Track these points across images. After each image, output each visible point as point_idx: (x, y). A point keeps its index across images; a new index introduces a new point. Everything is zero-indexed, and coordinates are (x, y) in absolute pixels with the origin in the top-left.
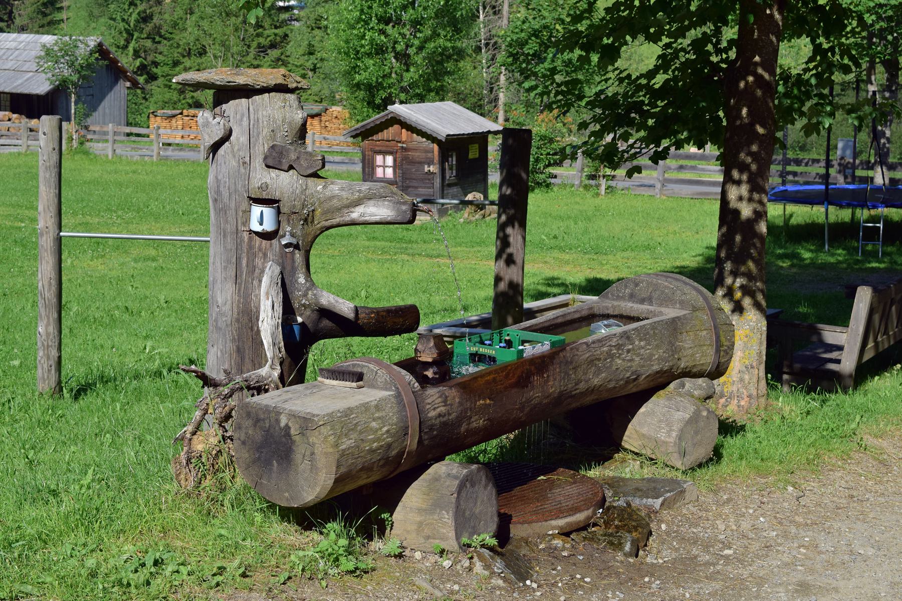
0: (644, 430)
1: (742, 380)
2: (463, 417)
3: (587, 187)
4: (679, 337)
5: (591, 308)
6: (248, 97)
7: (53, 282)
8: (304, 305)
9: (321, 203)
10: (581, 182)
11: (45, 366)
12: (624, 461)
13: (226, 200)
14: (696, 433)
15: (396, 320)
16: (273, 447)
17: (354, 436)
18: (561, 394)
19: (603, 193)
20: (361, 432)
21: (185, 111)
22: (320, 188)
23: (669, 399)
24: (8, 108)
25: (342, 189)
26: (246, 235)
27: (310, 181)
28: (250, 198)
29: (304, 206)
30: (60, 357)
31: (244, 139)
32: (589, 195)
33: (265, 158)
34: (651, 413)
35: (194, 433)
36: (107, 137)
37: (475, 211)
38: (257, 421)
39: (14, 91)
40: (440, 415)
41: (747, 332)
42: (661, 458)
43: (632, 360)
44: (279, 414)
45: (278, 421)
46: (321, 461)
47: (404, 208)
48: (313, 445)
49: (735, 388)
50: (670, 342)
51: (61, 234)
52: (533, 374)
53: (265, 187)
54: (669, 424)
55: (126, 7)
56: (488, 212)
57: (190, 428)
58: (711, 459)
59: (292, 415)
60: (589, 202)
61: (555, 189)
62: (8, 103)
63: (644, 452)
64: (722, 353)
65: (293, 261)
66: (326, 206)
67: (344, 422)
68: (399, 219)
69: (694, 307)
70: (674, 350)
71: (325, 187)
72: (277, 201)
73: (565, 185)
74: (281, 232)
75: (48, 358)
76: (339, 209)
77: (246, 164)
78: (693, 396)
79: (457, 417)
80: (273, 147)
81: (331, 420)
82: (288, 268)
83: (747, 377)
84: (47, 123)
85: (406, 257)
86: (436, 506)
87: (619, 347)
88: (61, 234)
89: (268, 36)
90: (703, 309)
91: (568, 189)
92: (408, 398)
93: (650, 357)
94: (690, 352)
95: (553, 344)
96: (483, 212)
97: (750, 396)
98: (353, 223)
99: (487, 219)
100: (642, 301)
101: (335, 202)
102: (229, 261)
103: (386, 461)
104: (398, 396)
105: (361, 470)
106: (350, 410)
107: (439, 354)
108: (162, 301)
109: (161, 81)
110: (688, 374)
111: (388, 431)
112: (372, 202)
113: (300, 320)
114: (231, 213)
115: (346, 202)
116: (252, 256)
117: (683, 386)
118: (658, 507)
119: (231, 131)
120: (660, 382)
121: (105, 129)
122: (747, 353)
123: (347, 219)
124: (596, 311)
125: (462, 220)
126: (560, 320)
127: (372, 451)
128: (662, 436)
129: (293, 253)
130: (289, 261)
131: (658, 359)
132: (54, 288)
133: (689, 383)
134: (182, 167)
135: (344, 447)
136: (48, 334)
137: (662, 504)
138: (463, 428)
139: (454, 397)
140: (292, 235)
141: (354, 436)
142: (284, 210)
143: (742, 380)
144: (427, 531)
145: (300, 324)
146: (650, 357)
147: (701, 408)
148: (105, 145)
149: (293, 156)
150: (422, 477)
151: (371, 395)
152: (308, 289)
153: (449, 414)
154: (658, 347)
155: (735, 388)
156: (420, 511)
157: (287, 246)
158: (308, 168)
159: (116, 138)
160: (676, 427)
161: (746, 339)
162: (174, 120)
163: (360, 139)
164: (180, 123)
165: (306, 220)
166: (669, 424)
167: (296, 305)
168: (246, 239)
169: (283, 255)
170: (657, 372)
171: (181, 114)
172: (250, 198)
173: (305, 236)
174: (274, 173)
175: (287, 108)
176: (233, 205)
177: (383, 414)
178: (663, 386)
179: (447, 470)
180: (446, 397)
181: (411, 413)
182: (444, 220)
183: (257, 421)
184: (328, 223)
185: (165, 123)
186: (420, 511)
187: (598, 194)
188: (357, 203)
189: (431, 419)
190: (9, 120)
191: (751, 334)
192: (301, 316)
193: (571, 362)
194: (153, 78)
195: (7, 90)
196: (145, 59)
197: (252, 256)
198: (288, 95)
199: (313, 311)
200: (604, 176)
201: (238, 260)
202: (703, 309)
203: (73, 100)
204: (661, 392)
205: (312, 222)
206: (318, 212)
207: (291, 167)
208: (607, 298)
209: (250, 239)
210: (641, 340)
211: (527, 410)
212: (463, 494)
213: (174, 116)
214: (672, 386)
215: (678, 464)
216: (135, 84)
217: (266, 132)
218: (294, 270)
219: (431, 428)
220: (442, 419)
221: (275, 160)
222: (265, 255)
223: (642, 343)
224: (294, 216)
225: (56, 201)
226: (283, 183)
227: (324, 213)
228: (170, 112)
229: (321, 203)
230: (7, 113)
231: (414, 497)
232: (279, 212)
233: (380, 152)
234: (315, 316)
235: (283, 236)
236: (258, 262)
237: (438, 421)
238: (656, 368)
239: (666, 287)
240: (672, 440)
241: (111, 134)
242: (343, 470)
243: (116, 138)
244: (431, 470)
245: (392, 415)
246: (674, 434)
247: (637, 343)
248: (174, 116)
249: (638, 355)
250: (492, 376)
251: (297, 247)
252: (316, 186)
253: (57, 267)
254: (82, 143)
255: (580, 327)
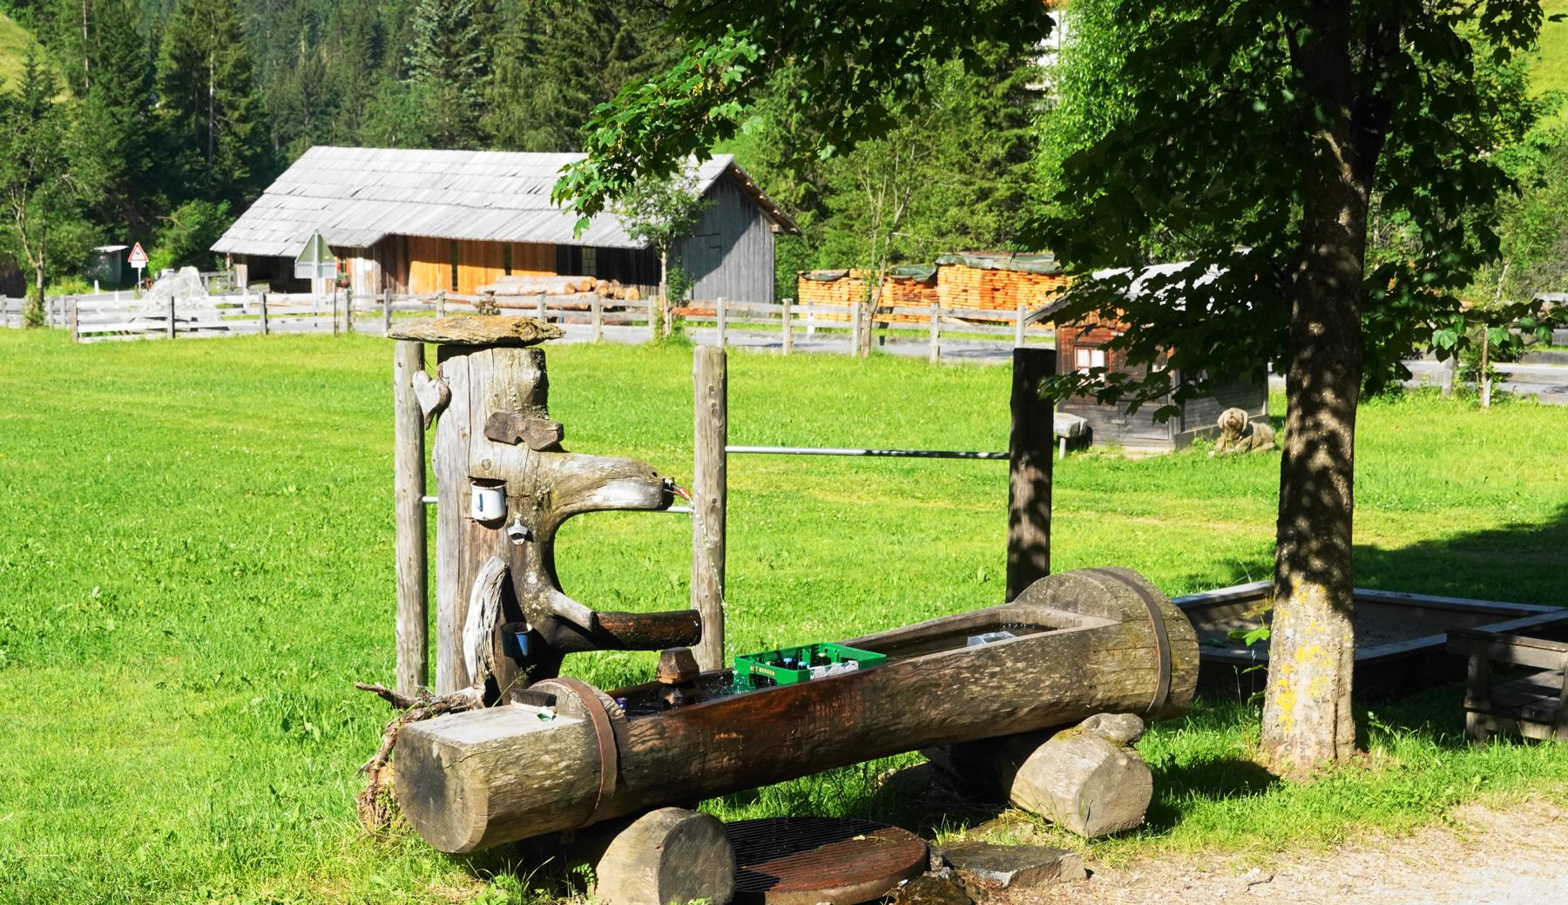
0: (1039, 783)
1: (1308, 719)
2: (686, 757)
3: (1462, 393)
4: (1093, 657)
5: (994, 615)
6: (468, 354)
7: (414, 564)
8: (535, 610)
9: (558, 484)
10: (1453, 385)
11: (405, 676)
12: (1013, 822)
13: (447, 480)
14: (1108, 789)
15: (666, 630)
16: (427, 782)
17: (514, 770)
18: (867, 731)
19: (1486, 402)
20: (525, 767)
21: (852, 271)
22: (556, 465)
23: (1075, 742)
24: (594, 271)
25: (583, 466)
26: (468, 523)
27: (544, 455)
28: (472, 479)
29: (535, 488)
30: (425, 666)
31: (464, 406)
32: (1463, 406)
33: (486, 429)
34: (1049, 760)
35: (382, 765)
36: (712, 319)
37: (1234, 439)
38: (414, 750)
39: (600, 244)
40: (651, 750)
41: (1318, 649)
42: (1057, 819)
43: (1000, 687)
44: (431, 742)
45: (430, 750)
46: (471, 799)
47: (652, 490)
48: (462, 780)
49: (1297, 731)
50: (1075, 664)
51: (425, 499)
52: (815, 703)
53: (487, 465)
54: (1070, 776)
55: (784, 101)
56: (1257, 440)
57: (378, 757)
58: (1142, 827)
59: (443, 745)
60: (1463, 416)
61: (1409, 398)
62: (593, 263)
63: (1038, 811)
64: (1175, 681)
65: (524, 556)
66: (564, 487)
67: (500, 755)
68: (647, 504)
69: (1124, 614)
70: (1080, 673)
71: (562, 464)
72: (503, 482)
73: (1426, 390)
74: (509, 520)
75: (409, 666)
76: (579, 492)
77: (467, 436)
78: (1108, 739)
79: (681, 754)
80: (495, 415)
81: (482, 752)
82: (518, 564)
83: (1315, 715)
84: (403, 351)
85: (1092, 515)
86: (642, 861)
87: (973, 669)
88: (425, 499)
89: (1007, 140)
90: (1145, 619)
91: (1431, 397)
92: (603, 728)
93: (1036, 684)
94: (1113, 677)
95: (862, 664)
96: (1247, 439)
97: (1320, 743)
98: (597, 509)
99: (1255, 451)
100: (1066, 606)
101: (574, 484)
102: (451, 555)
103: (568, 805)
104: (589, 724)
105: (531, 811)
106: (514, 740)
107: (682, 675)
108: (676, 583)
109: (836, 220)
110: (1112, 708)
111: (567, 767)
112: (615, 483)
113: (529, 627)
114: (452, 495)
115: (585, 483)
116: (475, 550)
117: (1097, 723)
118: (1006, 883)
119: (449, 395)
120: (1063, 717)
121: (712, 306)
122: (1316, 679)
123: (589, 503)
124: (1002, 618)
125: (1212, 453)
126: (933, 631)
127: (541, 789)
128: (1059, 791)
129: (524, 546)
130: (518, 556)
131: (1051, 687)
132: (415, 572)
133: (1106, 719)
134: (821, 365)
135: (498, 783)
136: (408, 634)
137: (1012, 880)
138: (694, 767)
139: (677, 729)
140: (523, 524)
141: (514, 770)
142: (512, 492)
143: (1308, 719)
144: (631, 892)
145: (528, 634)
146: (1036, 684)
147: (1118, 754)
148: (712, 330)
149: (521, 426)
150: (634, 825)
151: (563, 721)
152: (540, 591)
153: (668, 749)
154: (1049, 670)
155: (1297, 731)
156: (625, 866)
157: (516, 536)
158: (540, 440)
159: (728, 319)
160: (1079, 779)
161: (1315, 660)
162: (836, 285)
163: (1051, 324)
164: (845, 289)
165: (540, 504)
166: (1070, 776)
167: (527, 610)
168: (469, 529)
169: (512, 548)
170: (1052, 705)
171: (847, 275)
172: (472, 479)
173: (540, 525)
174: (498, 447)
175: (516, 367)
176: (454, 487)
177: (563, 746)
178: (1073, 723)
179: (660, 819)
180: (664, 728)
181: (607, 747)
182: (1187, 452)
183: (414, 750)
184: (568, 509)
185: (823, 290)
186: (625, 866)
187: (1477, 406)
188: (599, 484)
189: (638, 753)
190: (592, 289)
191: (1323, 653)
192: (532, 623)
193: (884, 688)
194: (824, 214)
195: (589, 243)
196: (814, 183)
197: (475, 550)
198: (517, 351)
199: (548, 617)
200: (1488, 376)
201: (461, 552)
202: (1145, 619)
203: (664, 261)
204: (1068, 731)
205: (549, 506)
206: (555, 495)
207: (519, 440)
208: (1024, 600)
209: (473, 528)
210: (1017, 660)
211: (806, 748)
212: (675, 848)
213: (836, 279)
214: (1085, 723)
215: (1079, 829)
216: (786, 225)
217: (488, 397)
218: (524, 566)
219: (638, 766)
220: (656, 756)
221: (499, 431)
222: (490, 548)
223: (1020, 665)
224: (524, 500)
225: (416, 454)
226: (510, 460)
227: (562, 496)
228: (830, 273)
229: (558, 484)
230: (588, 278)
231: (621, 848)
232: (504, 495)
233: (1083, 346)
234: (551, 623)
235: (512, 524)
236: (483, 556)
237: (649, 757)
238: (1047, 698)
239: (1095, 588)
240: (1070, 797)
241: (720, 313)
242: (498, 811)
243: (728, 319)
244: (644, 818)
245: (576, 748)
246: (1074, 789)
247: (1009, 664)
248: (836, 279)
249: (1013, 680)
250: (743, 704)
251: (529, 537)
252: (553, 462)
253: (419, 546)
254: (678, 329)
255: (714, 651)
